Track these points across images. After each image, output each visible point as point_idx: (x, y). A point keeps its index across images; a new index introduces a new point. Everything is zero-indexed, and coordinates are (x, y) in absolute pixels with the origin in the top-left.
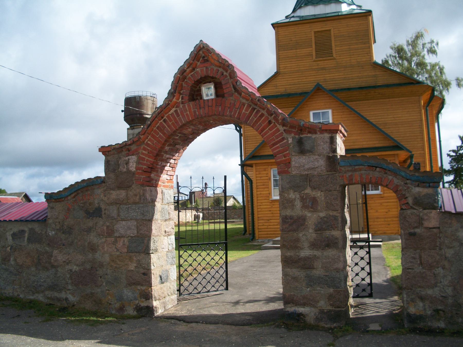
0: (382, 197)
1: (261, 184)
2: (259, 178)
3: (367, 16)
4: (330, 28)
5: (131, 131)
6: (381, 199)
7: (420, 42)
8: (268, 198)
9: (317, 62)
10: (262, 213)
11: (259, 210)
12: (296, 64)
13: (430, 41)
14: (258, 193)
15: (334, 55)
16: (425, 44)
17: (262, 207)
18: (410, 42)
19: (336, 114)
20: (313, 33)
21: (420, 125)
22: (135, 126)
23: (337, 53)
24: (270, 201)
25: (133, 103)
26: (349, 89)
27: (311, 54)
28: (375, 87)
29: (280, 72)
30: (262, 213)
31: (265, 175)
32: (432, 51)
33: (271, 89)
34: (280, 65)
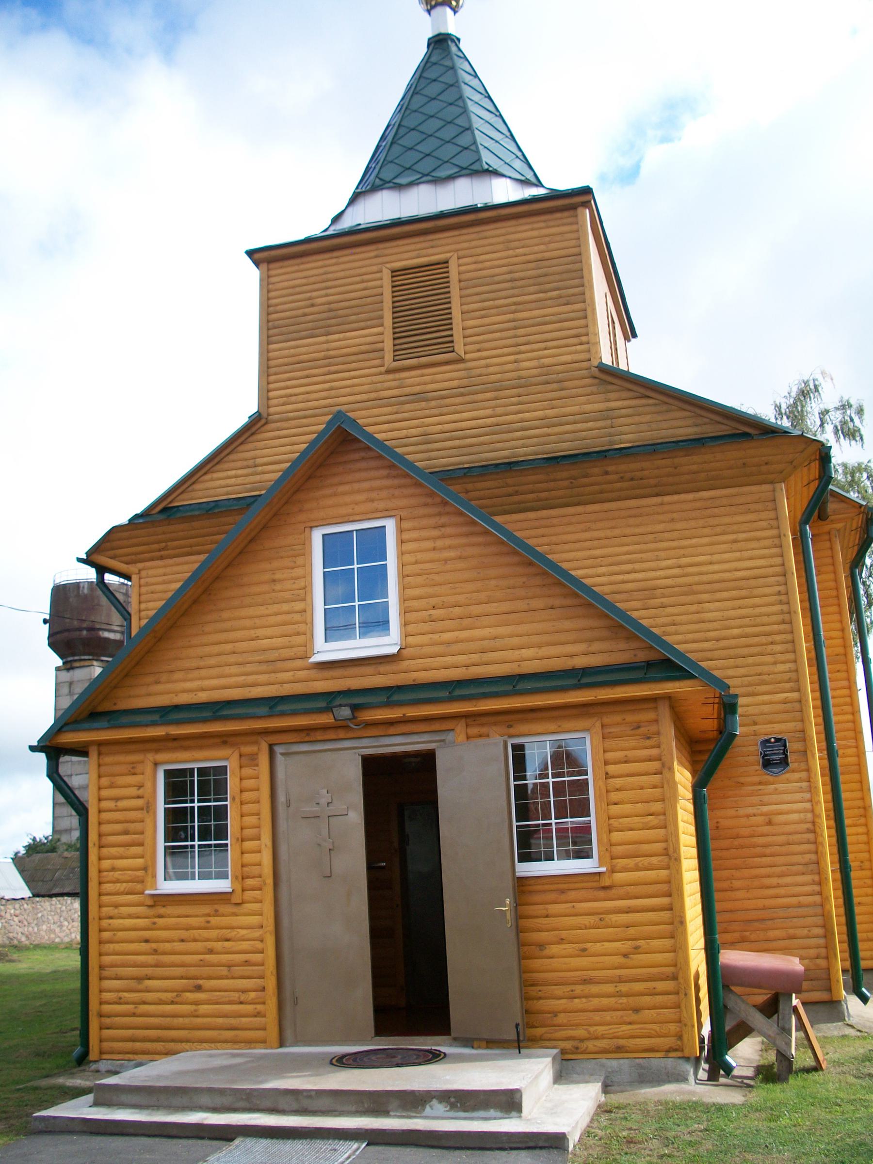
0: (605, 888)
1: (118, 827)
2: (110, 804)
3: (574, 207)
4: (448, 255)
5: (66, 676)
6: (602, 894)
7: (813, 408)
8: (139, 887)
9: (397, 376)
10: (117, 947)
11: (106, 935)
12: (327, 386)
13: (838, 404)
14: (106, 864)
15: (460, 348)
16: (827, 411)
17: (116, 922)
18: (784, 407)
19: (414, 535)
20: (386, 275)
21: (779, 593)
22: (75, 661)
23: (469, 340)
24: (150, 902)
25: (71, 600)
26: (510, 466)
27: (379, 346)
28: (603, 455)
29: (269, 415)
30: (117, 947)
31: (133, 791)
32: (850, 432)
33: (236, 477)
34: (268, 391)
